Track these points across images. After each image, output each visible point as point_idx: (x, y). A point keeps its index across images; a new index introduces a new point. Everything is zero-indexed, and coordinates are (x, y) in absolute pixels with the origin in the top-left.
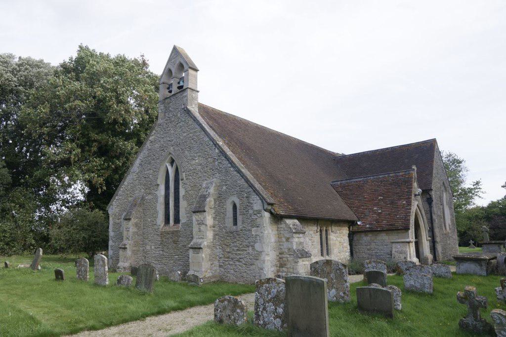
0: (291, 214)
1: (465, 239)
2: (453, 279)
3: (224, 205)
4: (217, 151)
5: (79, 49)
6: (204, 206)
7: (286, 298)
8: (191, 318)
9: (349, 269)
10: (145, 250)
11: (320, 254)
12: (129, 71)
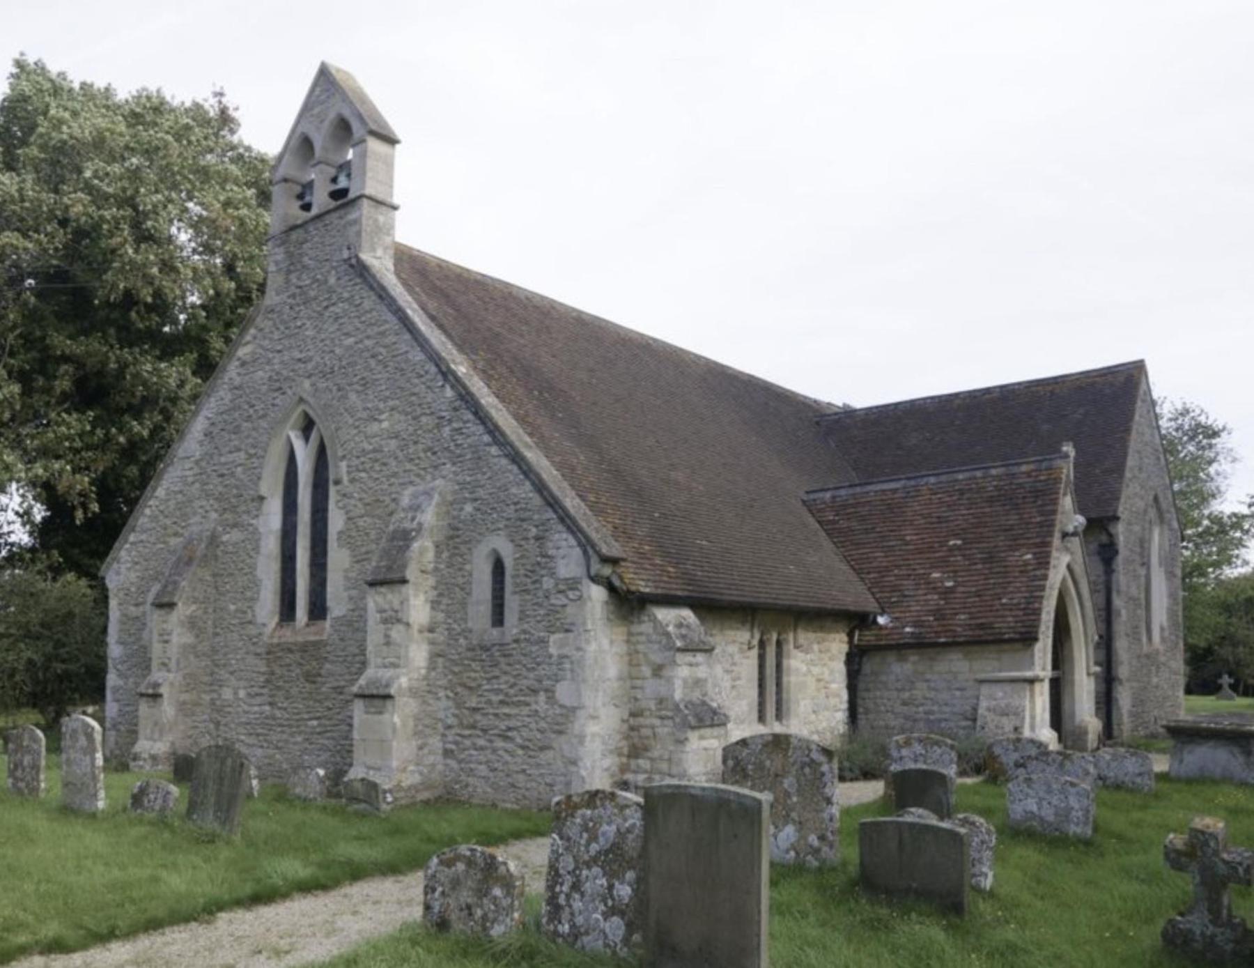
0: (673, 592)
1: (1204, 673)
2: (1157, 796)
3: (466, 562)
4: (449, 393)
5: (15, 70)
6: (404, 566)
7: (644, 852)
8: (355, 913)
9: (840, 762)
10: (218, 703)
11: (755, 715)
12: (173, 142)
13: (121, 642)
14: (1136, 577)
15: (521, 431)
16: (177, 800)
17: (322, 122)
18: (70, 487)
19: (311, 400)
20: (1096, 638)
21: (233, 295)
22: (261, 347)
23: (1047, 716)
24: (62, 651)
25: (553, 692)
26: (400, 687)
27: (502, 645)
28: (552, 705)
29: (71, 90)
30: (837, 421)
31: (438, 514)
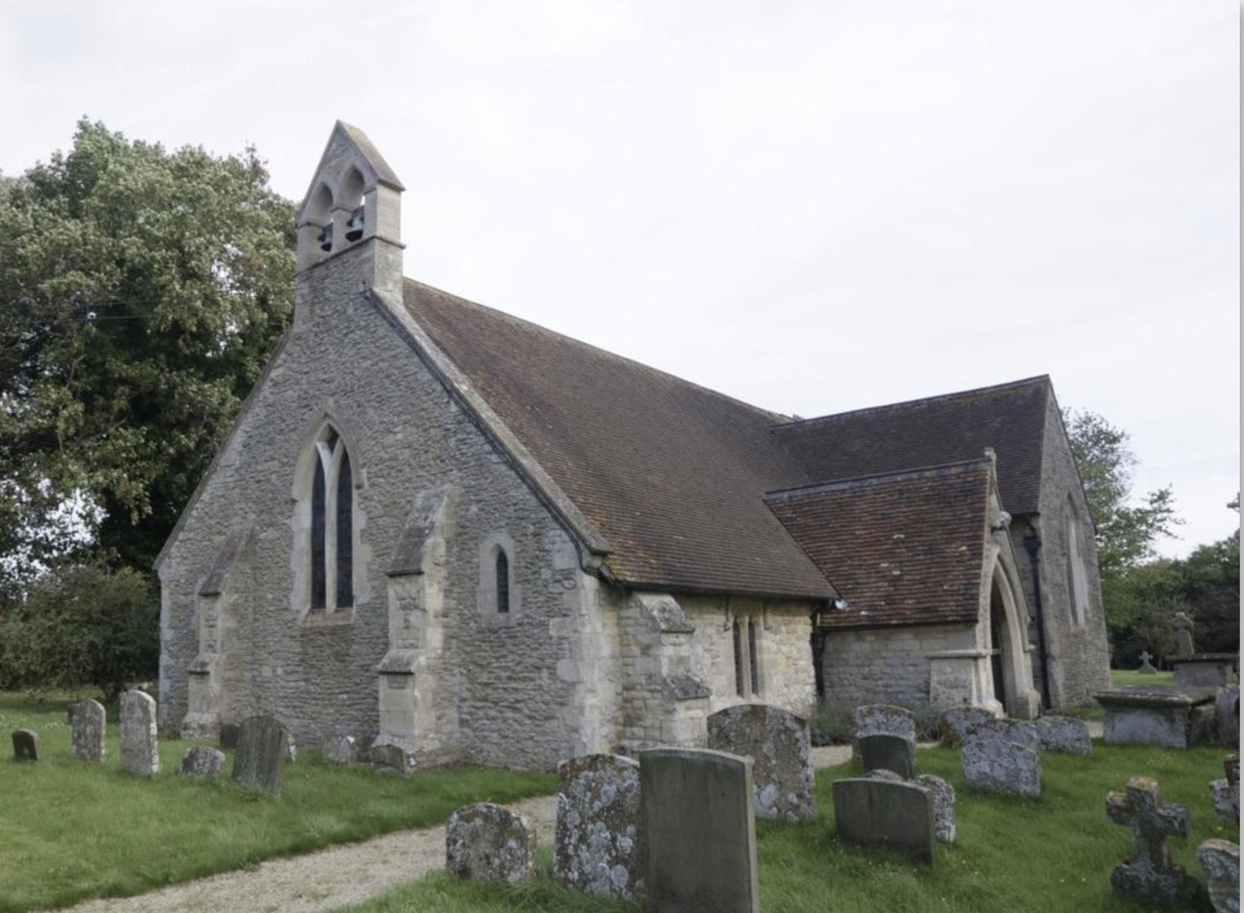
0: (656, 581)
1: (1127, 649)
4: (454, 408)
5: (79, 131)
6: (420, 560)
8: (385, 862)
9: (812, 730)
10: (259, 679)
11: (734, 689)
12: (213, 191)
13: (172, 627)
14: (1059, 566)
15: (517, 441)
16: (223, 764)
17: (339, 172)
18: (127, 492)
19: (335, 415)
20: (1029, 619)
21: (265, 324)
22: (291, 369)
23: (992, 688)
24: (120, 635)
25: (555, 669)
26: (419, 665)
27: (507, 628)
28: (554, 680)
29: (126, 148)
30: (789, 431)
31: (447, 514)
